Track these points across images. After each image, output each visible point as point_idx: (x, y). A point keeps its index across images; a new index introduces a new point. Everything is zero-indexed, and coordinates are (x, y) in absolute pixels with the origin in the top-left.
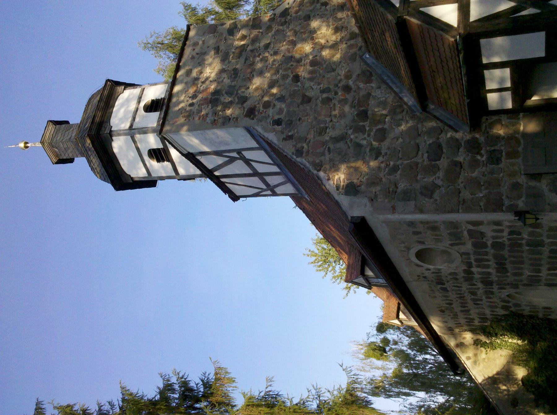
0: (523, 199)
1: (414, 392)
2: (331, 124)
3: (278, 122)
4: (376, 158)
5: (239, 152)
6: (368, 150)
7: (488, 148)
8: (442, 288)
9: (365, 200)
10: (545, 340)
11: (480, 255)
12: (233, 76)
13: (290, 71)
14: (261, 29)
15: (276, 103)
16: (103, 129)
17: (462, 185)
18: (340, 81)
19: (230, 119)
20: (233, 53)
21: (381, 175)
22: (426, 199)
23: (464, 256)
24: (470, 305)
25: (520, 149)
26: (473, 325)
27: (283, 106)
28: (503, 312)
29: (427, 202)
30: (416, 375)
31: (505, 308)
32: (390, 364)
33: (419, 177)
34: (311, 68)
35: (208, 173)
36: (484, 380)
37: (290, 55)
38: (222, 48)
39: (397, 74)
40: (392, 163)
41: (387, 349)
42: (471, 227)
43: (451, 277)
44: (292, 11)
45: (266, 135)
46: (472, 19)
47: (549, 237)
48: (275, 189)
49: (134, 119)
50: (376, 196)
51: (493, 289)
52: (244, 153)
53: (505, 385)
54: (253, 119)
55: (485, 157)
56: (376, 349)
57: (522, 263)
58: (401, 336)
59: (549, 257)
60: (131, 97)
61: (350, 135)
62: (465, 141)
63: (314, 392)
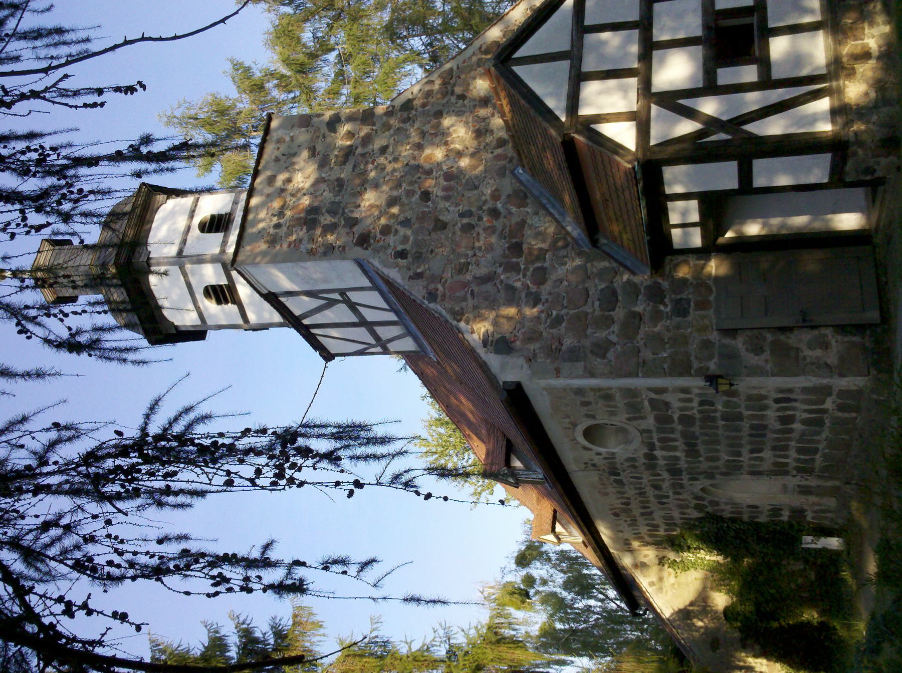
0: (715, 360)
1: (572, 659)
2: (474, 259)
3: (402, 254)
4: (534, 306)
5: (342, 292)
6: (523, 295)
7: (673, 296)
8: (615, 481)
9: (521, 361)
10: (752, 555)
11: (664, 432)
12: (337, 189)
13: (416, 185)
14: (374, 125)
15: (399, 228)
16: (136, 254)
17: (641, 343)
18: (485, 202)
19: (334, 248)
20: (336, 156)
21: (542, 327)
22: (598, 360)
23: (644, 435)
24: (654, 505)
25: (712, 298)
26: (657, 536)
27: (409, 232)
28: (695, 514)
29: (598, 363)
30: (573, 632)
31: (698, 508)
32: (535, 615)
33: (589, 331)
34: (445, 183)
35: (292, 320)
36: (672, 614)
37: (416, 163)
38: (319, 148)
39: (561, 201)
40: (554, 313)
41: (532, 592)
42: (653, 396)
43: (628, 464)
44: (417, 103)
45: (386, 271)
46: (653, 142)
47: (748, 409)
48: (388, 345)
49: (184, 242)
50: (535, 355)
51: (682, 479)
52: (349, 294)
53: (702, 621)
54: (366, 249)
55: (669, 307)
56: (514, 593)
57: (718, 442)
58: (552, 571)
59: (751, 435)
60: (178, 208)
61: (499, 275)
62: (646, 287)
63: (441, 632)
